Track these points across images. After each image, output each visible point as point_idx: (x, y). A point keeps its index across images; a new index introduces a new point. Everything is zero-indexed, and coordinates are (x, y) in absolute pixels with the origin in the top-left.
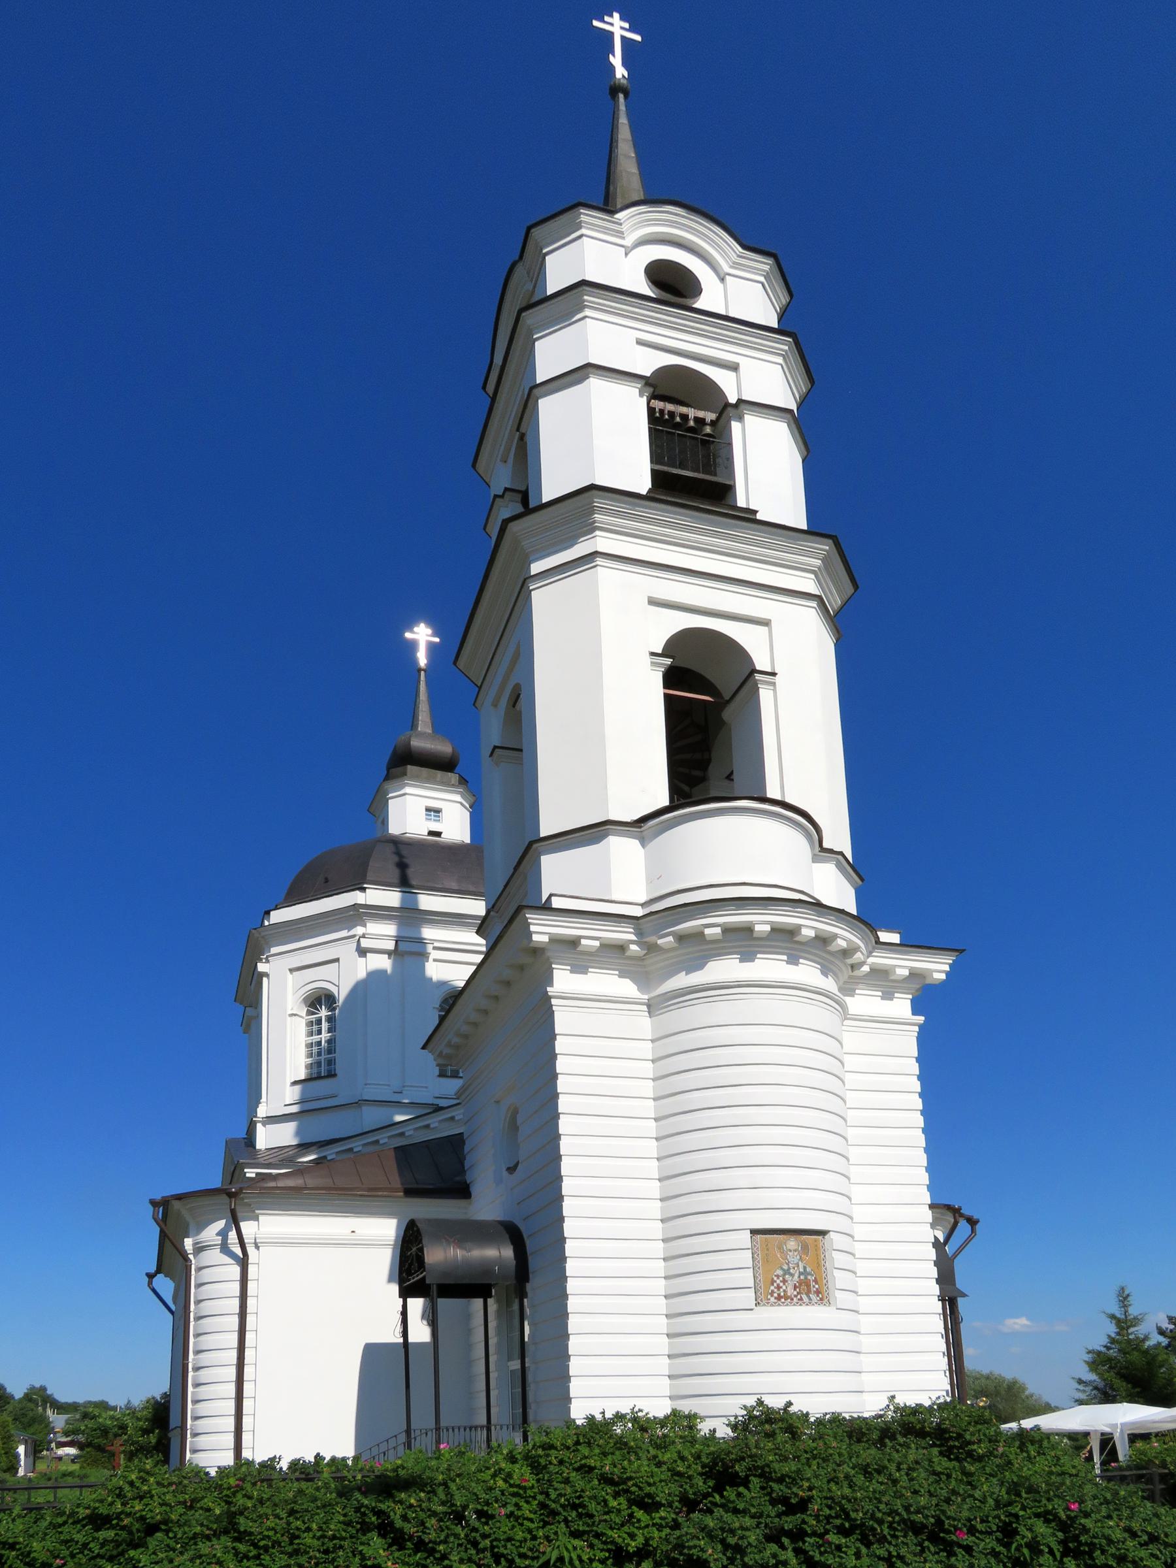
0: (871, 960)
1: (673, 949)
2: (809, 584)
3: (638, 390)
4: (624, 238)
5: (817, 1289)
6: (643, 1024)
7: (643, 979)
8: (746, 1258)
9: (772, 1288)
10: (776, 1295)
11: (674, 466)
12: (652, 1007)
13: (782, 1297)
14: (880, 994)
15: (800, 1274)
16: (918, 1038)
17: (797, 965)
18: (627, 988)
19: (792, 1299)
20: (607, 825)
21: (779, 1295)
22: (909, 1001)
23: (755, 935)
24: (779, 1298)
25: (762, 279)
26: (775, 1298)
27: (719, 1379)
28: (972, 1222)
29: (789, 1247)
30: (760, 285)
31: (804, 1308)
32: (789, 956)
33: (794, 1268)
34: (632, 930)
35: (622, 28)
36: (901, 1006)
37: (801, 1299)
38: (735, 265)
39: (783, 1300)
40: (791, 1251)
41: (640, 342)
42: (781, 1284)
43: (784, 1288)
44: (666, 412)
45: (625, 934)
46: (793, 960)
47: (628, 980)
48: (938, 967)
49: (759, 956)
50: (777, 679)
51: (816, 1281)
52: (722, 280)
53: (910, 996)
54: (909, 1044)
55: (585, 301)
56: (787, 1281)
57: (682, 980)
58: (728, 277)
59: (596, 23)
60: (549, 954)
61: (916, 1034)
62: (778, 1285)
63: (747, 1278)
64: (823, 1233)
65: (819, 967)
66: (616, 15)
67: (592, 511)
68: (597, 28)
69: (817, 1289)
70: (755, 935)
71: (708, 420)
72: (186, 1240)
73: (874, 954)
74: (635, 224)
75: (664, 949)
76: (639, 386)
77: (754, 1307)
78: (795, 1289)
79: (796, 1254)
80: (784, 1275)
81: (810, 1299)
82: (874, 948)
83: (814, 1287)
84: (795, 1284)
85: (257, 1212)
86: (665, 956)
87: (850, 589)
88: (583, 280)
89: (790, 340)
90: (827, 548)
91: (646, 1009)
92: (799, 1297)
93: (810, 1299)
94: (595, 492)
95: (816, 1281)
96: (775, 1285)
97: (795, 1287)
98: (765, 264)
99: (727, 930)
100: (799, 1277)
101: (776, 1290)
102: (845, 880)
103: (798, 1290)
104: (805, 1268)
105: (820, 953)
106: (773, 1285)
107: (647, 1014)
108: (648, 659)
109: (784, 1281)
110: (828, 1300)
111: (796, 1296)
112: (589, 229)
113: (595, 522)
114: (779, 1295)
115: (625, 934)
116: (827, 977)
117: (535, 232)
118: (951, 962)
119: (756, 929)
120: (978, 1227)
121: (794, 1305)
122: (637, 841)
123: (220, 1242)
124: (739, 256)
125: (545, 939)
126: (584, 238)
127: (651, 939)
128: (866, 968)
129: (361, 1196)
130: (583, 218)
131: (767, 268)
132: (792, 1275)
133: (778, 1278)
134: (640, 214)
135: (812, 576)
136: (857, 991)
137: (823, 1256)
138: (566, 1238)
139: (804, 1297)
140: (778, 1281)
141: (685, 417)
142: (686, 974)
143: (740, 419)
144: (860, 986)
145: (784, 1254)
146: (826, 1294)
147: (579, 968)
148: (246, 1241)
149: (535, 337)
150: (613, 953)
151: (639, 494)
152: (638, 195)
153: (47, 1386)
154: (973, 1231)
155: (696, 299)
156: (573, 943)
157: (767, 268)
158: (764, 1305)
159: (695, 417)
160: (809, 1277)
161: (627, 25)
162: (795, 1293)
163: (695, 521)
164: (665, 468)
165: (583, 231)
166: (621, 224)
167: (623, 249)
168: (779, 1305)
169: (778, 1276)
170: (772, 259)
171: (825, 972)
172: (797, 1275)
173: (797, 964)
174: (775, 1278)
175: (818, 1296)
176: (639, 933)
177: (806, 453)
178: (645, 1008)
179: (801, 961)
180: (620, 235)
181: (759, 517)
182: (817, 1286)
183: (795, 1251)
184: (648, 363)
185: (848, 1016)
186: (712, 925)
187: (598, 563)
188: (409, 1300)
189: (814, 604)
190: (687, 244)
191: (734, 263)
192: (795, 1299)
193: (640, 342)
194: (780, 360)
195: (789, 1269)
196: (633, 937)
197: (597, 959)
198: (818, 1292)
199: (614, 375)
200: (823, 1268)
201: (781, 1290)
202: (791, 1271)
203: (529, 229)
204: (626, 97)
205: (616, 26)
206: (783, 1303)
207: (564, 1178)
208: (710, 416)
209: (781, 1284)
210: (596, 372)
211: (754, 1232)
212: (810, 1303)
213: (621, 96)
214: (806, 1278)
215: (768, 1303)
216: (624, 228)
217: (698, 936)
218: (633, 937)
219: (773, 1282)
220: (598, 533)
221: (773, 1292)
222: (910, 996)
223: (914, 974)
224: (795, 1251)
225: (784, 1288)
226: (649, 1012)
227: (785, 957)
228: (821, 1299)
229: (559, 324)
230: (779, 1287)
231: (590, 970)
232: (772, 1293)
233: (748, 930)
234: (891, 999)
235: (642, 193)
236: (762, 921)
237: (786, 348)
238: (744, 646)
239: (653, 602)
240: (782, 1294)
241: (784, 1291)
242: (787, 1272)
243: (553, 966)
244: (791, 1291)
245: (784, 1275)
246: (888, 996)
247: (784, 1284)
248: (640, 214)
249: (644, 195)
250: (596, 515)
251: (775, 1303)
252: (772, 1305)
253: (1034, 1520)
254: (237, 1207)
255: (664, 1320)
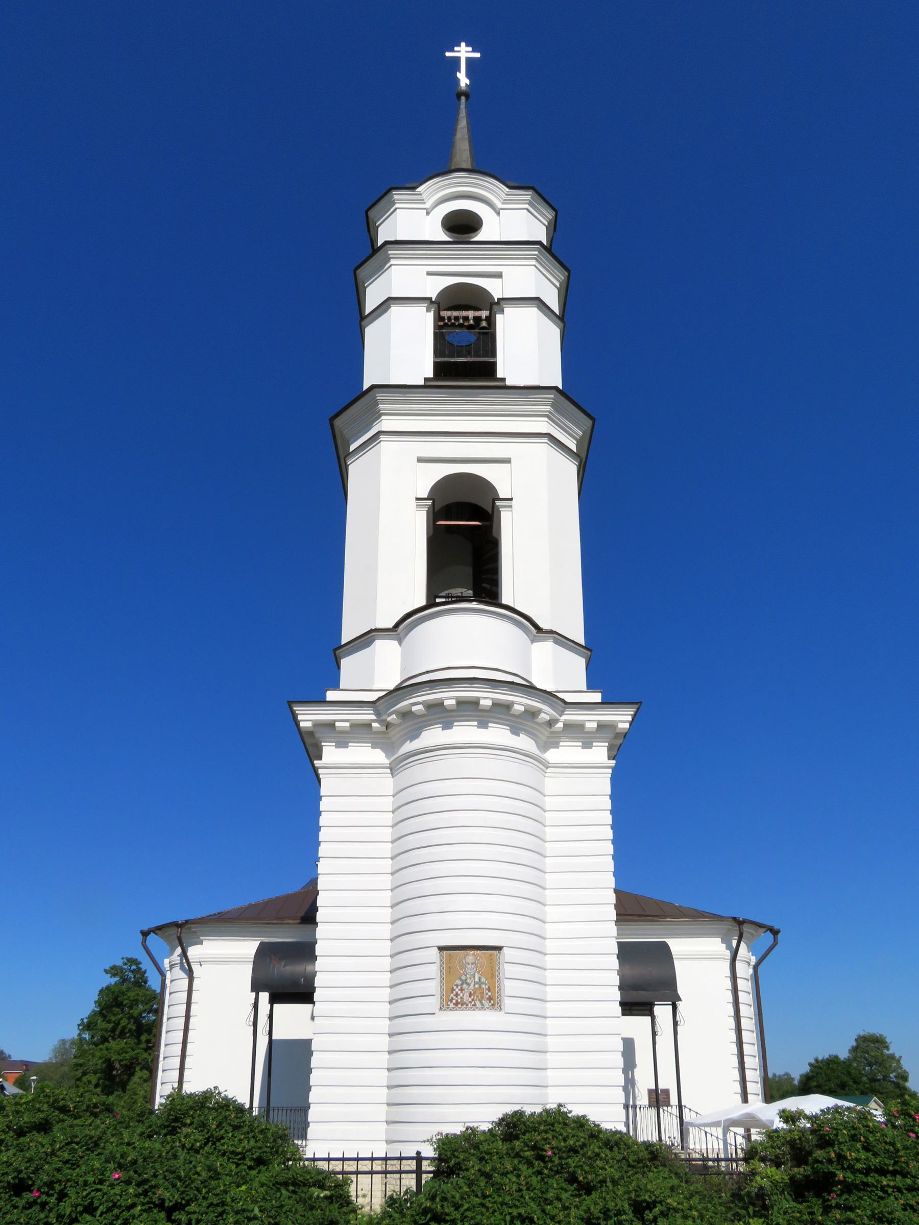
0: (564, 718)
1: (399, 725)
2: (542, 425)
3: (425, 308)
4: (425, 203)
5: (490, 996)
6: (387, 783)
7: (388, 747)
8: (433, 970)
9: (452, 995)
10: (454, 1001)
11: (453, 356)
12: (393, 769)
13: (459, 1003)
14: (580, 744)
15: (476, 983)
16: (611, 779)
17: (487, 729)
18: (378, 756)
19: (467, 1005)
20: (372, 633)
21: (457, 1001)
22: (606, 748)
23: (480, 708)
24: (457, 1004)
25: (527, 206)
26: (454, 1004)
27: (427, 1072)
28: (775, 932)
29: (468, 960)
30: (526, 211)
31: (477, 1013)
32: (479, 723)
33: (470, 979)
34: (372, 712)
35: (466, 52)
36: (600, 753)
37: (475, 1005)
38: (505, 202)
39: (460, 1006)
40: (469, 964)
41: (429, 274)
42: (459, 992)
43: (461, 995)
44: (453, 317)
45: (367, 715)
46: (483, 725)
47: (379, 750)
48: (622, 718)
49: (455, 724)
50: (513, 503)
51: (489, 990)
52: (498, 214)
53: (607, 744)
54: (604, 784)
55: (389, 254)
56: (464, 990)
57: (409, 747)
58: (501, 211)
59: (448, 54)
60: (317, 735)
61: (610, 775)
62: (457, 993)
63: (433, 987)
64: (499, 949)
65: (508, 728)
66: (463, 44)
67: (376, 403)
68: (448, 57)
69: (490, 996)
70: (480, 708)
71: (484, 317)
72: (165, 960)
73: (566, 712)
74: (430, 194)
75: (395, 725)
76: (426, 305)
77: (437, 1010)
78: (470, 997)
79: (473, 966)
80: (462, 984)
81: (482, 1004)
82: (565, 708)
83: (487, 994)
84: (471, 992)
85: (201, 938)
86: (398, 729)
87: (589, 423)
88: (386, 241)
89: (538, 246)
90: (552, 396)
91: (390, 772)
92: (473, 1003)
93: (482, 1004)
94: (376, 390)
95: (489, 990)
96: (454, 992)
97: (470, 995)
98: (527, 195)
99: (461, 703)
100: (474, 986)
101: (454, 997)
102: (566, 651)
103: (472, 997)
104: (480, 978)
105: (506, 717)
106: (453, 993)
107: (390, 775)
108: (414, 503)
109: (462, 990)
110: (500, 1006)
111: (470, 1002)
112: (400, 203)
113: (380, 410)
114: (457, 1001)
115: (367, 715)
116: (519, 736)
117: (371, 213)
118: (633, 713)
119: (481, 703)
120: (779, 936)
121: (468, 1010)
122: (396, 642)
123: (179, 962)
124: (507, 195)
125: (309, 724)
126: (397, 210)
127: (384, 717)
128: (560, 725)
129: (268, 924)
130: (396, 197)
131: (529, 197)
132: (469, 984)
133: (457, 987)
134: (435, 184)
135: (546, 419)
136: (561, 744)
137: (497, 968)
138: (317, 956)
139: (478, 1003)
140: (457, 990)
141: (466, 318)
142: (410, 742)
143: (502, 312)
144: (563, 739)
145: (463, 967)
146: (497, 1000)
147: (342, 744)
148: (190, 961)
149: (366, 285)
150: (360, 731)
151: (406, 385)
152: (467, 165)
153: (789, 1072)
154: (775, 940)
155: (477, 232)
156: (331, 725)
157: (529, 197)
158: (445, 1010)
159: (474, 317)
160: (483, 986)
161: (470, 49)
162: (470, 1000)
163: (450, 396)
164: (446, 359)
165: (397, 206)
166: (421, 195)
167: (425, 211)
168: (457, 1010)
169: (457, 985)
170: (532, 190)
171: (515, 731)
172: (472, 984)
173: (487, 727)
174: (455, 987)
175: (490, 1002)
176: (378, 714)
177: (562, 325)
178: (388, 771)
179: (490, 725)
180: (422, 201)
181: (508, 383)
182: (489, 994)
183: (473, 964)
184: (433, 288)
185: (550, 765)
186: (416, 703)
187: (381, 439)
188: (275, 1005)
189: (546, 440)
190: (482, 197)
191: (505, 200)
192: (469, 1005)
193: (429, 274)
194: (534, 262)
195: (466, 980)
196: (373, 717)
197: (352, 736)
198: (490, 999)
199: (407, 302)
200: (497, 979)
201: (459, 997)
202: (468, 981)
203: (367, 212)
204: (467, 99)
205: (464, 52)
206: (460, 1008)
207: (319, 908)
208: (484, 314)
209: (459, 992)
210: (394, 302)
211: (441, 949)
212: (483, 1008)
213: (463, 98)
214: (480, 987)
215: (448, 1008)
216: (424, 196)
217: (406, 715)
218: (373, 717)
219: (453, 990)
220: (383, 417)
221: (452, 999)
222: (607, 744)
223: (602, 727)
224: (473, 964)
225: (461, 995)
226: (392, 774)
227: (476, 723)
228: (493, 1005)
229: (376, 274)
230: (457, 995)
231: (350, 744)
232: (451, 1001)
233: (475, 703)
234: (591, 747)
235: (469, 162)
236: (449, 697)
237: (537, 253)
238: (489, 480)
239: (420, 460)
240: (459, 1001)
241: (461, 998)
242: (464, 982)
243: (323, 744)
244: (466, 998)
245: (462, 984)
246: (587, 745)
247: (462, 992)
248: (435, 184)
249: (472, 163)
250: (380, 406)
251: (453, 1008)
252: (451, 1010)
253: (62, 1187)
254: (182, 935)
255: (387, 1022)
